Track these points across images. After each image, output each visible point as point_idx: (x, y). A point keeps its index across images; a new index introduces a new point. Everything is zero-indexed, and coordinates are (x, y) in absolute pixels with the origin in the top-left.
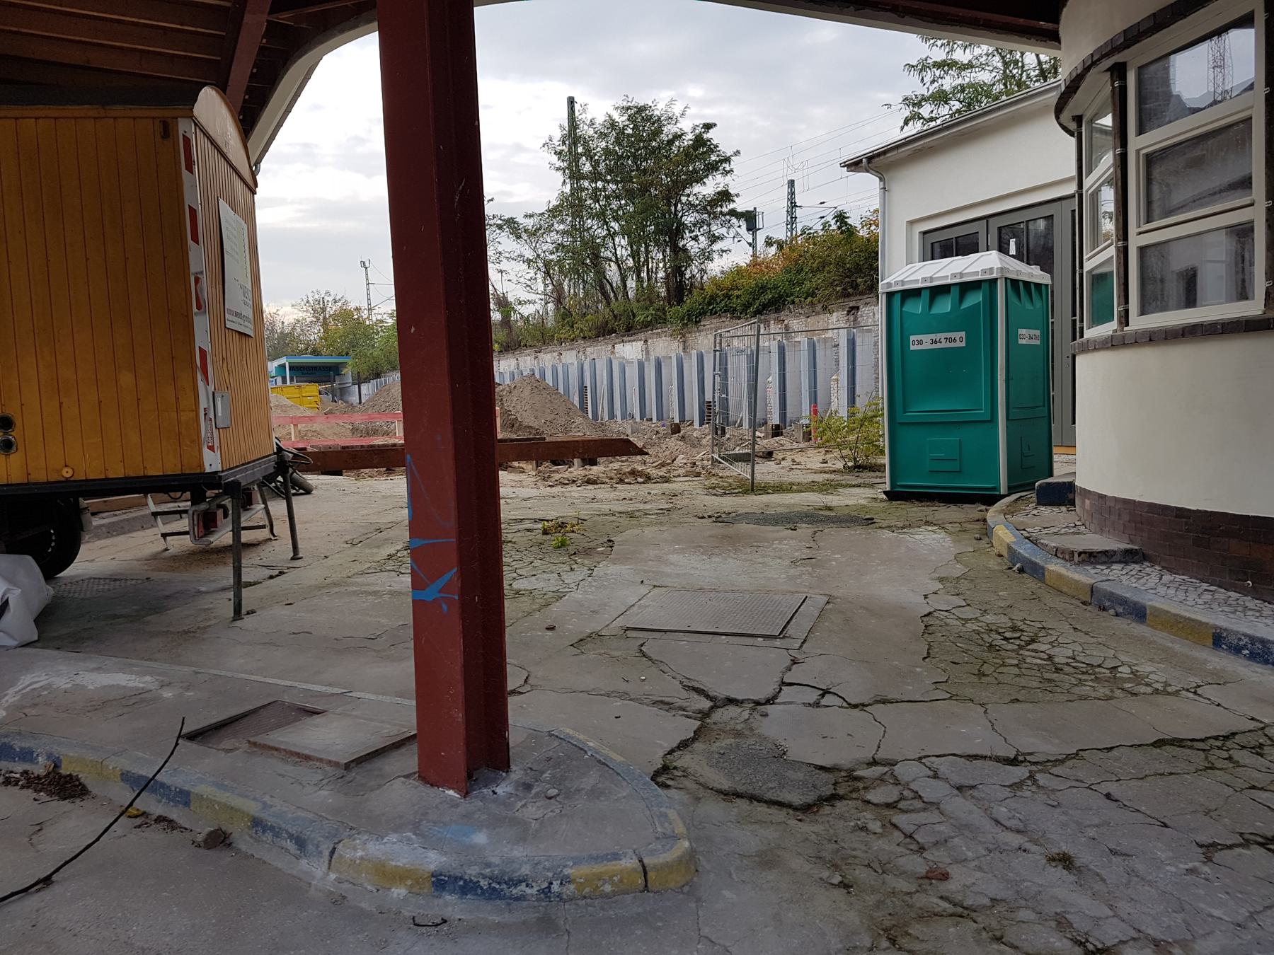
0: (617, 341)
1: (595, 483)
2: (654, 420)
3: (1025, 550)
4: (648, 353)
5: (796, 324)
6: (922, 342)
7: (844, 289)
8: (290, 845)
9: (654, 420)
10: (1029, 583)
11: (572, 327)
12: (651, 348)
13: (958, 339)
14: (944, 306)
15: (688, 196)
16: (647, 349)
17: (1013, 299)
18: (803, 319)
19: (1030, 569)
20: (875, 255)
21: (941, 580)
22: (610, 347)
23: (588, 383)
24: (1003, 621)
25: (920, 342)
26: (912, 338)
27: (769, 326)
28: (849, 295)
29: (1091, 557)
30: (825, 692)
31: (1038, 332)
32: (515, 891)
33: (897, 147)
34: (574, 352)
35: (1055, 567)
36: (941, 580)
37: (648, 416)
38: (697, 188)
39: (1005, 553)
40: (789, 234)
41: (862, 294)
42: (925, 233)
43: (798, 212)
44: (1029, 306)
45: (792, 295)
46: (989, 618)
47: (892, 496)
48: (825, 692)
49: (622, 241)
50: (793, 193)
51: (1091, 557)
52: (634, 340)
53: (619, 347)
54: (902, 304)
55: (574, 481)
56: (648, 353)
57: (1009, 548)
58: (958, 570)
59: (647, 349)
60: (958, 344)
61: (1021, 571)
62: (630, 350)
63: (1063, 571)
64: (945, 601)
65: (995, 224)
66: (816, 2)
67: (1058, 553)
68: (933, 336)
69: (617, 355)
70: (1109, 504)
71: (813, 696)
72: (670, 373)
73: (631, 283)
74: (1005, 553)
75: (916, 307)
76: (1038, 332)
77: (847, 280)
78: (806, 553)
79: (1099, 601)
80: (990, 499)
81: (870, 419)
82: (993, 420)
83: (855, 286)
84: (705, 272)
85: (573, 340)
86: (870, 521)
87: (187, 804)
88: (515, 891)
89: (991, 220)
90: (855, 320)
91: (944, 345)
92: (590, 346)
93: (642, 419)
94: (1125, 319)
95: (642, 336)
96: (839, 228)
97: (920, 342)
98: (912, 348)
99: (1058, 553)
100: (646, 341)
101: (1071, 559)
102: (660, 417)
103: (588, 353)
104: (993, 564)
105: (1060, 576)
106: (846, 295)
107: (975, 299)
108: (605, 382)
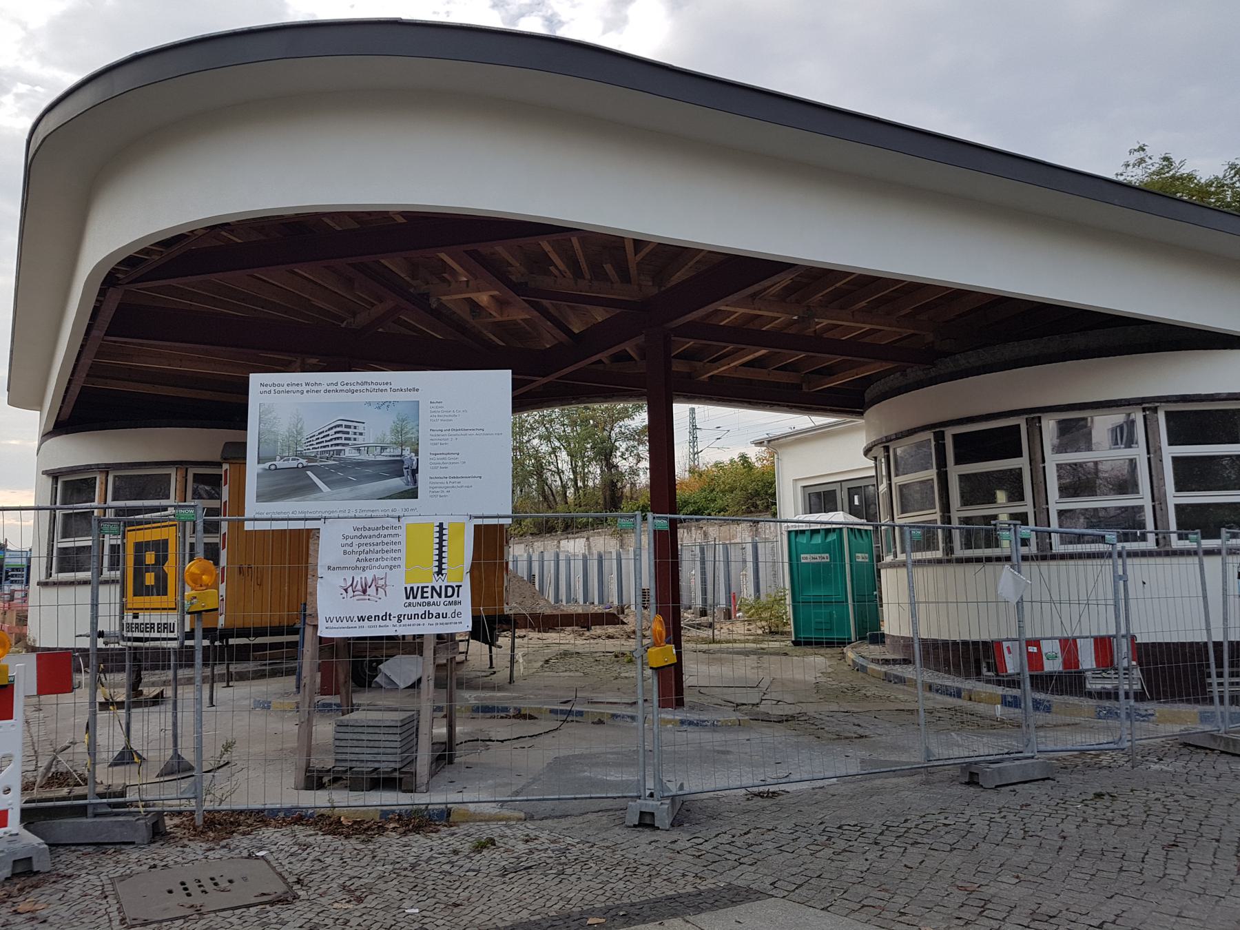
0: (562, 537)
1: (612, 637)
2: (596, 602)
3: (861, 661)
4: (590, 548)
5: (713, 531)
6: (806, 558)
7: (748, 508)
8: (629, 720)
9: (596, 602)
10: (861, 674)
11: (520, 524)
12: (592, 544)
13: (825, 559)
14: (818, 540)
15: (621, 427)
16: (589, 545)
17: (852, 538)
18: (716, 527)
19: (863, 669)
20: (772, 484)
21: (822, 673)
22: (556, 542)
23: (536, 571)
24: (847, 685)
25: (806, 558)
26: (802, 556)
27: (691, 531)
28: (751, 512)
29: (886, 662)
30: (779, 701)
31: (867, 555)
32: (704, 724)
33: (786, 437)
34: (523, 546)
35: (873, 666)
36: (822, 673)
37: (590, 600)
38: (627, 422)
39: (851, 664)
40: (691, 450)
41: (760, 512)
42: (804, 487)
43: (699, 433)
44: (861, 541)
45: (708, 508)
46: (842, 684)
47: (796, 643)
48: (779, 701)
49: (564, 455)
50: (694, 418)
51: (886, 662)
52: (577, 538)
53: (563, 543)
54: (796, 538)
55: (599, 637)
56: (590, 548)
57: (853, 661)
58: (830, 670)
59: (589, 545)
60: (826, 560)
61: (858, 670)
62: (574, 546)
63: (874, 667)
64: (823, 679)
65: (846, 486)
66: (749, 403)
67: (873, 661)
68: (813, 555)
69: (562, 549)
70: (896, 639)
71: (775, 702)
72: (611, 566)
73: (570, 492)
74: (851, 664)
75: (803, 540)
76: (867, 555)
77: (750, 501)
78: (756, 665)
79: (888, 678)
80: (843, 643)
81: (779, 601)
82: (847, 601)
83: (756, 506)
84: (635, 485)
85: (521, 536)
86: (786, 654)
87: (582, 715)
88: (704, 724)
89: (843, 483)
90: (757, 530)
91: (818, 560)
92: (537, 541)
93: (585, 602)
94: (896, 556)
95: (585, 534)
96: (743, 464)
97: (806, 558)
98: (803, 561)
99: (873, 661)
100: (588, 539)
101: (878, 663)
102: (601, 602)
103: (535, 547)
104: (846, 668)
105: (874, 670)
106: (749, 512)
107: (832, 537)
108: (552, 571)
